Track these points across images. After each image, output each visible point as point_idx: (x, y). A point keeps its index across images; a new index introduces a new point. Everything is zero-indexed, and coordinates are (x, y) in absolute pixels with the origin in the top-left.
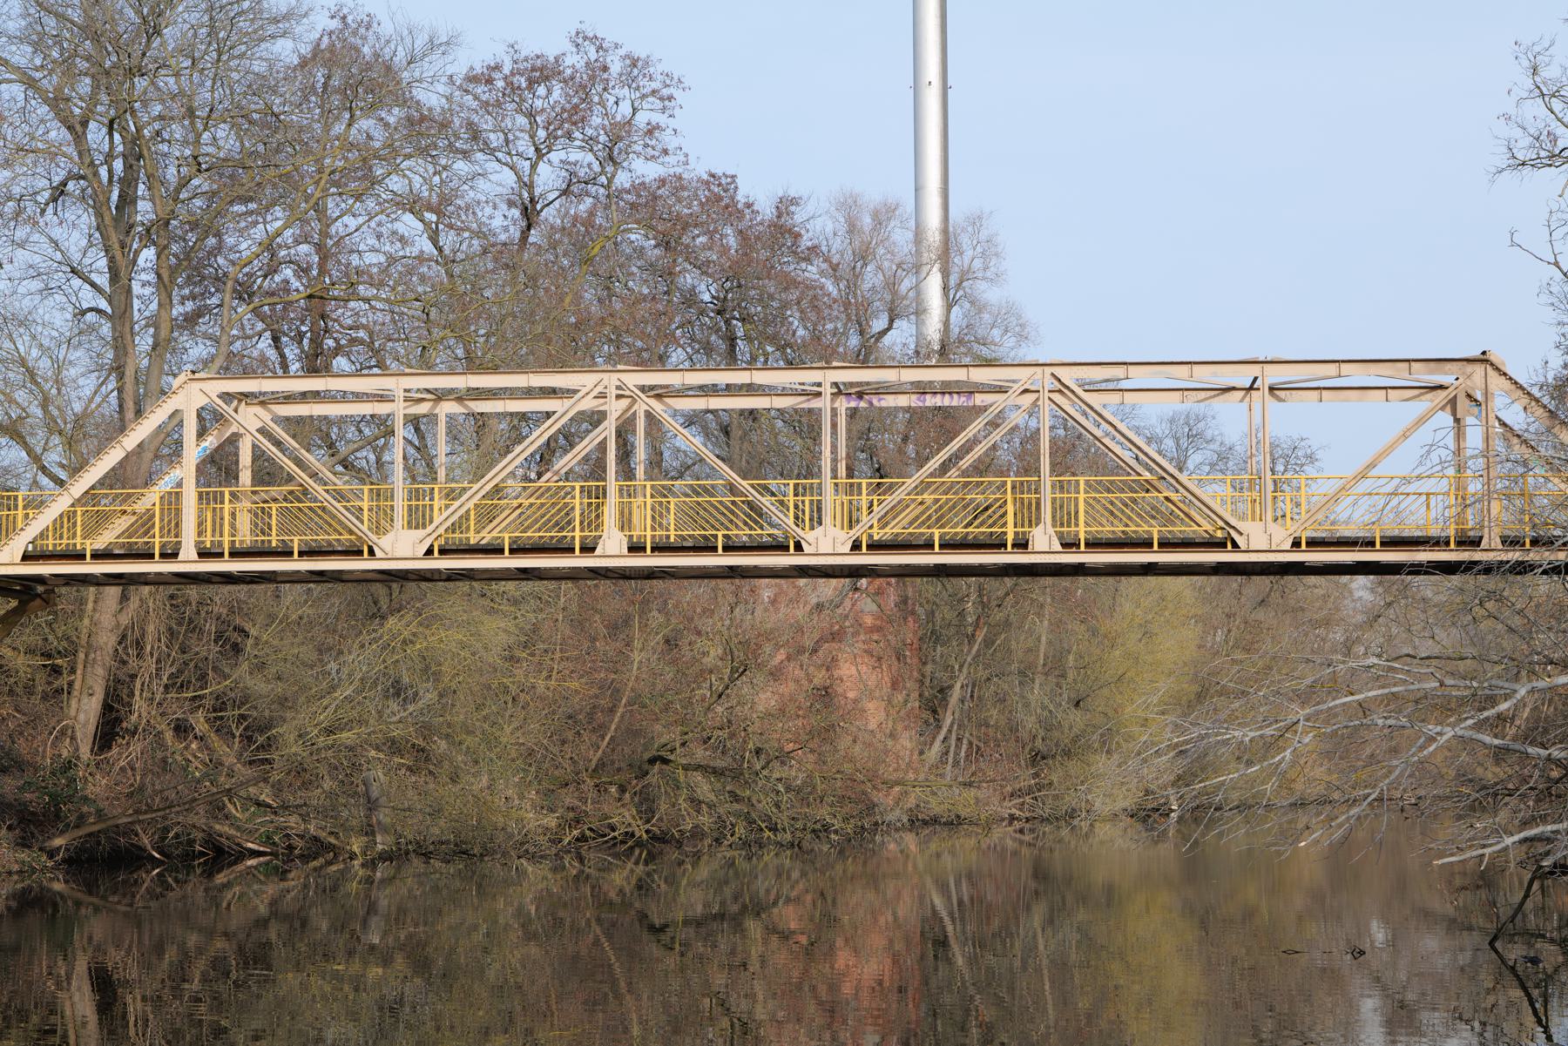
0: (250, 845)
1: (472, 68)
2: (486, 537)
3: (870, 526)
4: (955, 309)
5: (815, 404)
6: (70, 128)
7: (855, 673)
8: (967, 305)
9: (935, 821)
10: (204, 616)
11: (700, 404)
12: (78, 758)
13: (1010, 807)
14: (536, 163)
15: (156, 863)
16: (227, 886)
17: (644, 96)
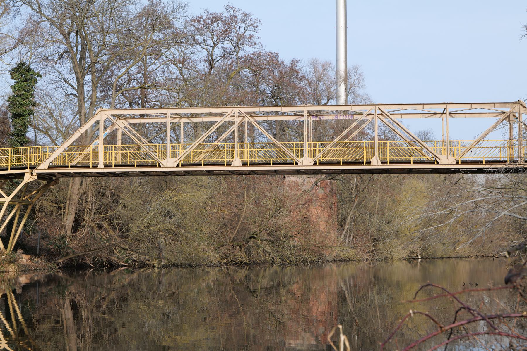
0: (121, 263)
1: (193, 17)
2: (197, 160)
3: (319, 156)
4: (349, 96)
5: (302, 119)
6: (63, 35)
7: (316, 212)
8: (353, 95)
9: (341, 260)
10: (107, 185)
11: (265, 119)
12: (67, 235)
13: (366, 256)
14: (214, 48)
15: (91, 267)
16: (113, 276)
17: (248, 26)
